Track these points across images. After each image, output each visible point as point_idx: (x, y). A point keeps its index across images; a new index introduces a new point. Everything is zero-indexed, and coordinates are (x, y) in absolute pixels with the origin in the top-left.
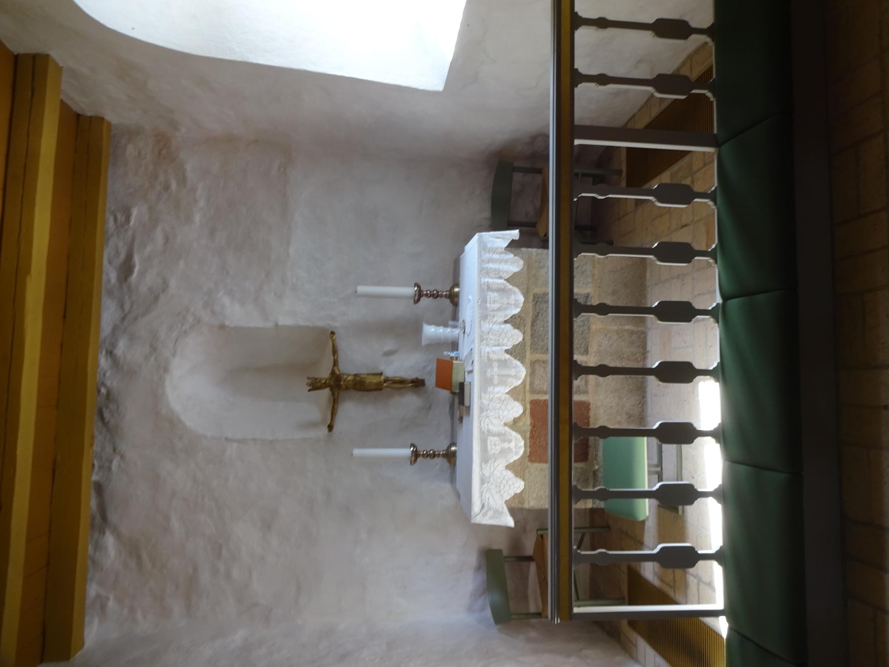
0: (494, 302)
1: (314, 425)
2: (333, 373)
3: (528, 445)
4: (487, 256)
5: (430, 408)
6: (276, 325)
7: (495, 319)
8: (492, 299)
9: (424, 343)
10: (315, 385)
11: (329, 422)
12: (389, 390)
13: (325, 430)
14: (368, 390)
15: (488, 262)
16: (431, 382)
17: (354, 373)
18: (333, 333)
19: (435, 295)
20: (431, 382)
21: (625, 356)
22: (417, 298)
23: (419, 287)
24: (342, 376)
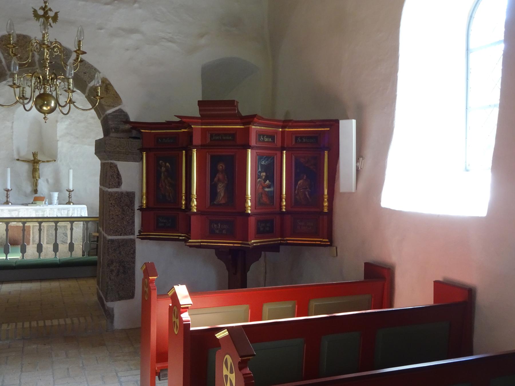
0: (64, 212)
1: (19, 153)
2: (40, 161)
3: (15, 225)
4: (79, 210)
5: (26, 196)
6: (58, 141)
7: (58, 213)
8: (65, 212)
9: (51, 193)
10: (34, 155)
11: (20, 159)
12: (33, 181)
13: (17, 158)
14: (33, 172)
15: (77, 210)
16: (36, 195)
17: (39, 168)
18: (55, 161)
19: (70, 197)
20: (36, 195)
21: (46, 257)
22: (68, 190)
23: (73, 191)
24: (38, 164)
